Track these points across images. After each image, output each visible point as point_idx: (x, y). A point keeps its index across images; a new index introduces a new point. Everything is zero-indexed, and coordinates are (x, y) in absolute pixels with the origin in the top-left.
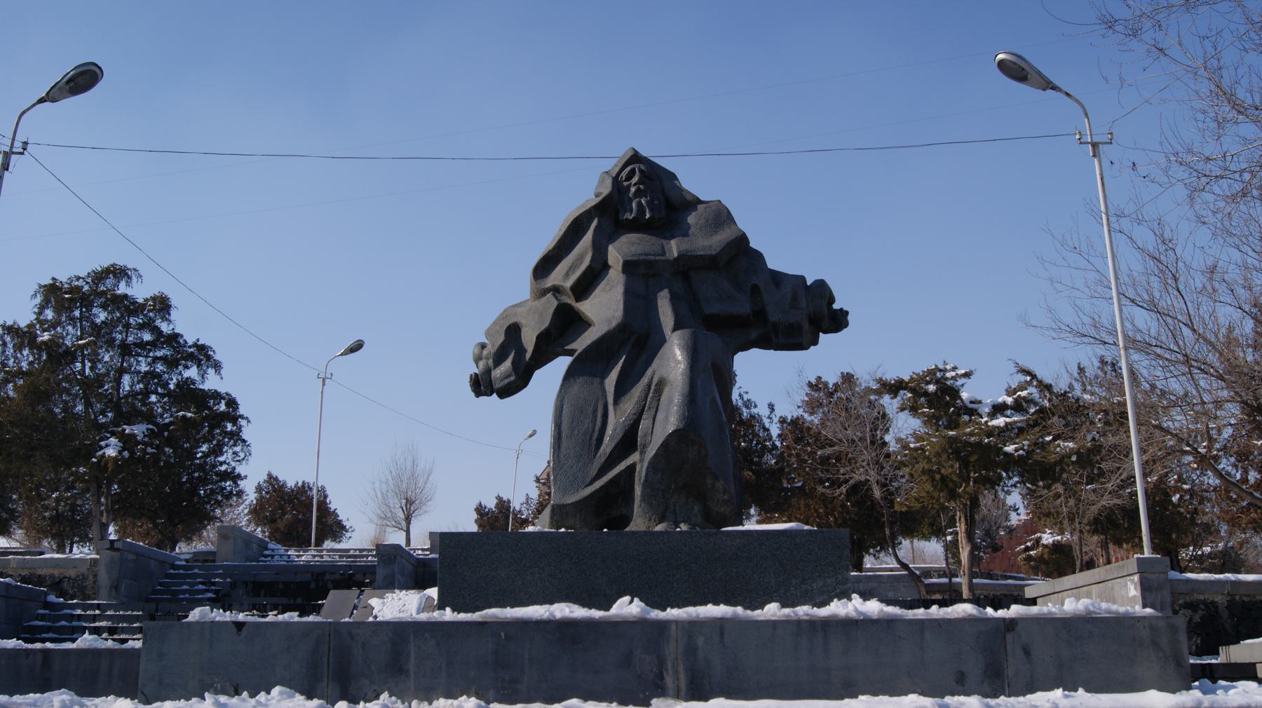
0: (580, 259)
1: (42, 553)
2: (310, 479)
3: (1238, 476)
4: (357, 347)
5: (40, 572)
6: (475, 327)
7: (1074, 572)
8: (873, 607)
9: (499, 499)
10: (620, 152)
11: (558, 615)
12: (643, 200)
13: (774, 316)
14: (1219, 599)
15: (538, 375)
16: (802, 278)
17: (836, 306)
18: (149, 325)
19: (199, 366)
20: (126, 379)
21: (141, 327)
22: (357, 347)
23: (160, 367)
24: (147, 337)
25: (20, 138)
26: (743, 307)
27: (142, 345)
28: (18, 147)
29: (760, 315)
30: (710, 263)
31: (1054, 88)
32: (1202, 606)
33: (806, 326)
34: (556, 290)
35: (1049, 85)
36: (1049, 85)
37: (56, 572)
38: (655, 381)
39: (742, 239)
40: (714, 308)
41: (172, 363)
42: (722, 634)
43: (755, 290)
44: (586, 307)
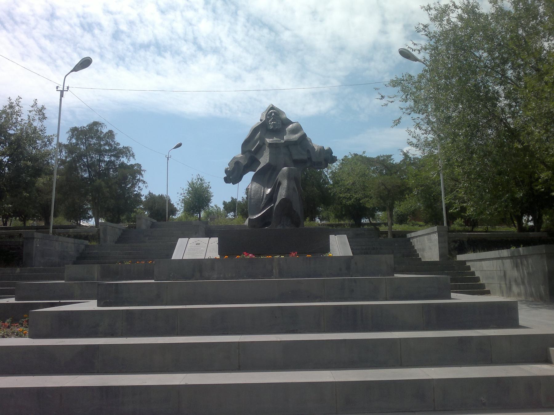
1: (55, 216)
2: (164, 194)
4: (179, 145)
9: (232, 198)
13: (314, 159)
15: (245, 177)
16: (133, 173)
18: (107, 144)
19: (127, 156)
21: (105, 145)
22: (179, 145)
23: (113, 158)
24: (107, 148)
25: (66, 85)
26: (305, 157)
27: (106, 151)
28: (65, 89)
29: (310, 159)
34: (250, 151)
37: (86, 234)
39: (304, 136)
40: (296, 157)
41: (117, 156)
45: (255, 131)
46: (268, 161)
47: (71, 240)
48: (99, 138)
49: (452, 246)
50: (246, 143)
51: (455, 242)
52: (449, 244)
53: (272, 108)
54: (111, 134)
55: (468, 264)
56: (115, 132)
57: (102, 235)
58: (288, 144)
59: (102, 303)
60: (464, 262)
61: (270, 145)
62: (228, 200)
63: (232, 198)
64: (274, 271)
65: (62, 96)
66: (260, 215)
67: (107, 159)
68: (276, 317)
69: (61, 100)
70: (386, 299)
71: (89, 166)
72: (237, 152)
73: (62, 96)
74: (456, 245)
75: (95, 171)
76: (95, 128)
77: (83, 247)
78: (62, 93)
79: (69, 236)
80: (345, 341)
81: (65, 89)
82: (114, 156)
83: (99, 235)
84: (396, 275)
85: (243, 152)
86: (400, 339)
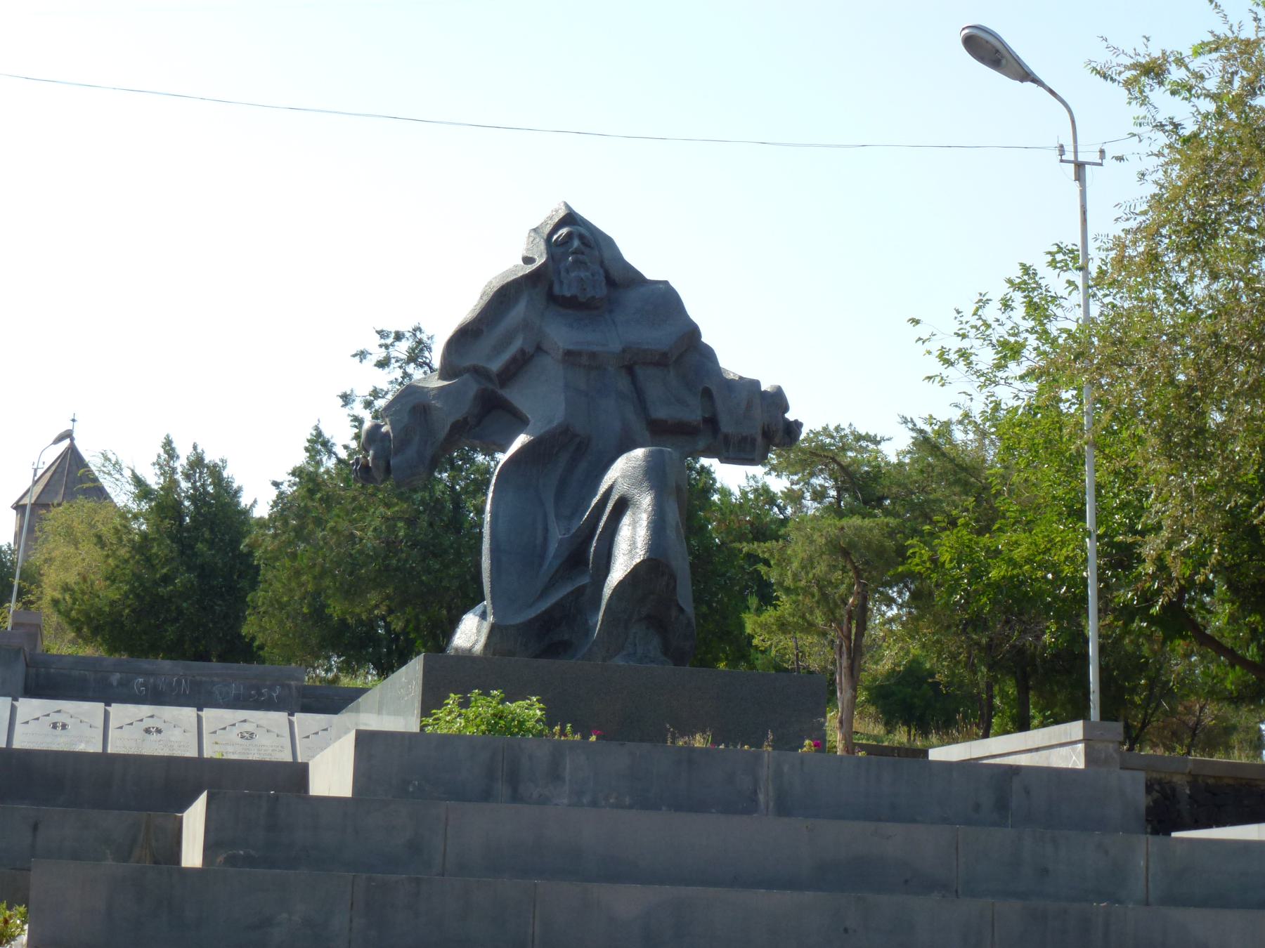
3: (1167, 241)
7: (986, 735)
10: (545, 212)
11: (120, 744)
12: (576, 279)
13: (726, 426)
14: (1178, 780)
16: (756, 384)
17: (790, 416)
20: (889, 612)
26: (694, 413)
29: (712, 422)
30: (662, 361)
31: (1036, 80)
32: (1157, 787)
33: (759, 439)
34: (478, 372)
35: (1025, 75)
36: (1025, 75)
43: (707, 393)
44: (517, 396)
45: (503, 298)
53: (570, 218)
61: (571, 357)
64: (761, 797)
66: (1093, 650)
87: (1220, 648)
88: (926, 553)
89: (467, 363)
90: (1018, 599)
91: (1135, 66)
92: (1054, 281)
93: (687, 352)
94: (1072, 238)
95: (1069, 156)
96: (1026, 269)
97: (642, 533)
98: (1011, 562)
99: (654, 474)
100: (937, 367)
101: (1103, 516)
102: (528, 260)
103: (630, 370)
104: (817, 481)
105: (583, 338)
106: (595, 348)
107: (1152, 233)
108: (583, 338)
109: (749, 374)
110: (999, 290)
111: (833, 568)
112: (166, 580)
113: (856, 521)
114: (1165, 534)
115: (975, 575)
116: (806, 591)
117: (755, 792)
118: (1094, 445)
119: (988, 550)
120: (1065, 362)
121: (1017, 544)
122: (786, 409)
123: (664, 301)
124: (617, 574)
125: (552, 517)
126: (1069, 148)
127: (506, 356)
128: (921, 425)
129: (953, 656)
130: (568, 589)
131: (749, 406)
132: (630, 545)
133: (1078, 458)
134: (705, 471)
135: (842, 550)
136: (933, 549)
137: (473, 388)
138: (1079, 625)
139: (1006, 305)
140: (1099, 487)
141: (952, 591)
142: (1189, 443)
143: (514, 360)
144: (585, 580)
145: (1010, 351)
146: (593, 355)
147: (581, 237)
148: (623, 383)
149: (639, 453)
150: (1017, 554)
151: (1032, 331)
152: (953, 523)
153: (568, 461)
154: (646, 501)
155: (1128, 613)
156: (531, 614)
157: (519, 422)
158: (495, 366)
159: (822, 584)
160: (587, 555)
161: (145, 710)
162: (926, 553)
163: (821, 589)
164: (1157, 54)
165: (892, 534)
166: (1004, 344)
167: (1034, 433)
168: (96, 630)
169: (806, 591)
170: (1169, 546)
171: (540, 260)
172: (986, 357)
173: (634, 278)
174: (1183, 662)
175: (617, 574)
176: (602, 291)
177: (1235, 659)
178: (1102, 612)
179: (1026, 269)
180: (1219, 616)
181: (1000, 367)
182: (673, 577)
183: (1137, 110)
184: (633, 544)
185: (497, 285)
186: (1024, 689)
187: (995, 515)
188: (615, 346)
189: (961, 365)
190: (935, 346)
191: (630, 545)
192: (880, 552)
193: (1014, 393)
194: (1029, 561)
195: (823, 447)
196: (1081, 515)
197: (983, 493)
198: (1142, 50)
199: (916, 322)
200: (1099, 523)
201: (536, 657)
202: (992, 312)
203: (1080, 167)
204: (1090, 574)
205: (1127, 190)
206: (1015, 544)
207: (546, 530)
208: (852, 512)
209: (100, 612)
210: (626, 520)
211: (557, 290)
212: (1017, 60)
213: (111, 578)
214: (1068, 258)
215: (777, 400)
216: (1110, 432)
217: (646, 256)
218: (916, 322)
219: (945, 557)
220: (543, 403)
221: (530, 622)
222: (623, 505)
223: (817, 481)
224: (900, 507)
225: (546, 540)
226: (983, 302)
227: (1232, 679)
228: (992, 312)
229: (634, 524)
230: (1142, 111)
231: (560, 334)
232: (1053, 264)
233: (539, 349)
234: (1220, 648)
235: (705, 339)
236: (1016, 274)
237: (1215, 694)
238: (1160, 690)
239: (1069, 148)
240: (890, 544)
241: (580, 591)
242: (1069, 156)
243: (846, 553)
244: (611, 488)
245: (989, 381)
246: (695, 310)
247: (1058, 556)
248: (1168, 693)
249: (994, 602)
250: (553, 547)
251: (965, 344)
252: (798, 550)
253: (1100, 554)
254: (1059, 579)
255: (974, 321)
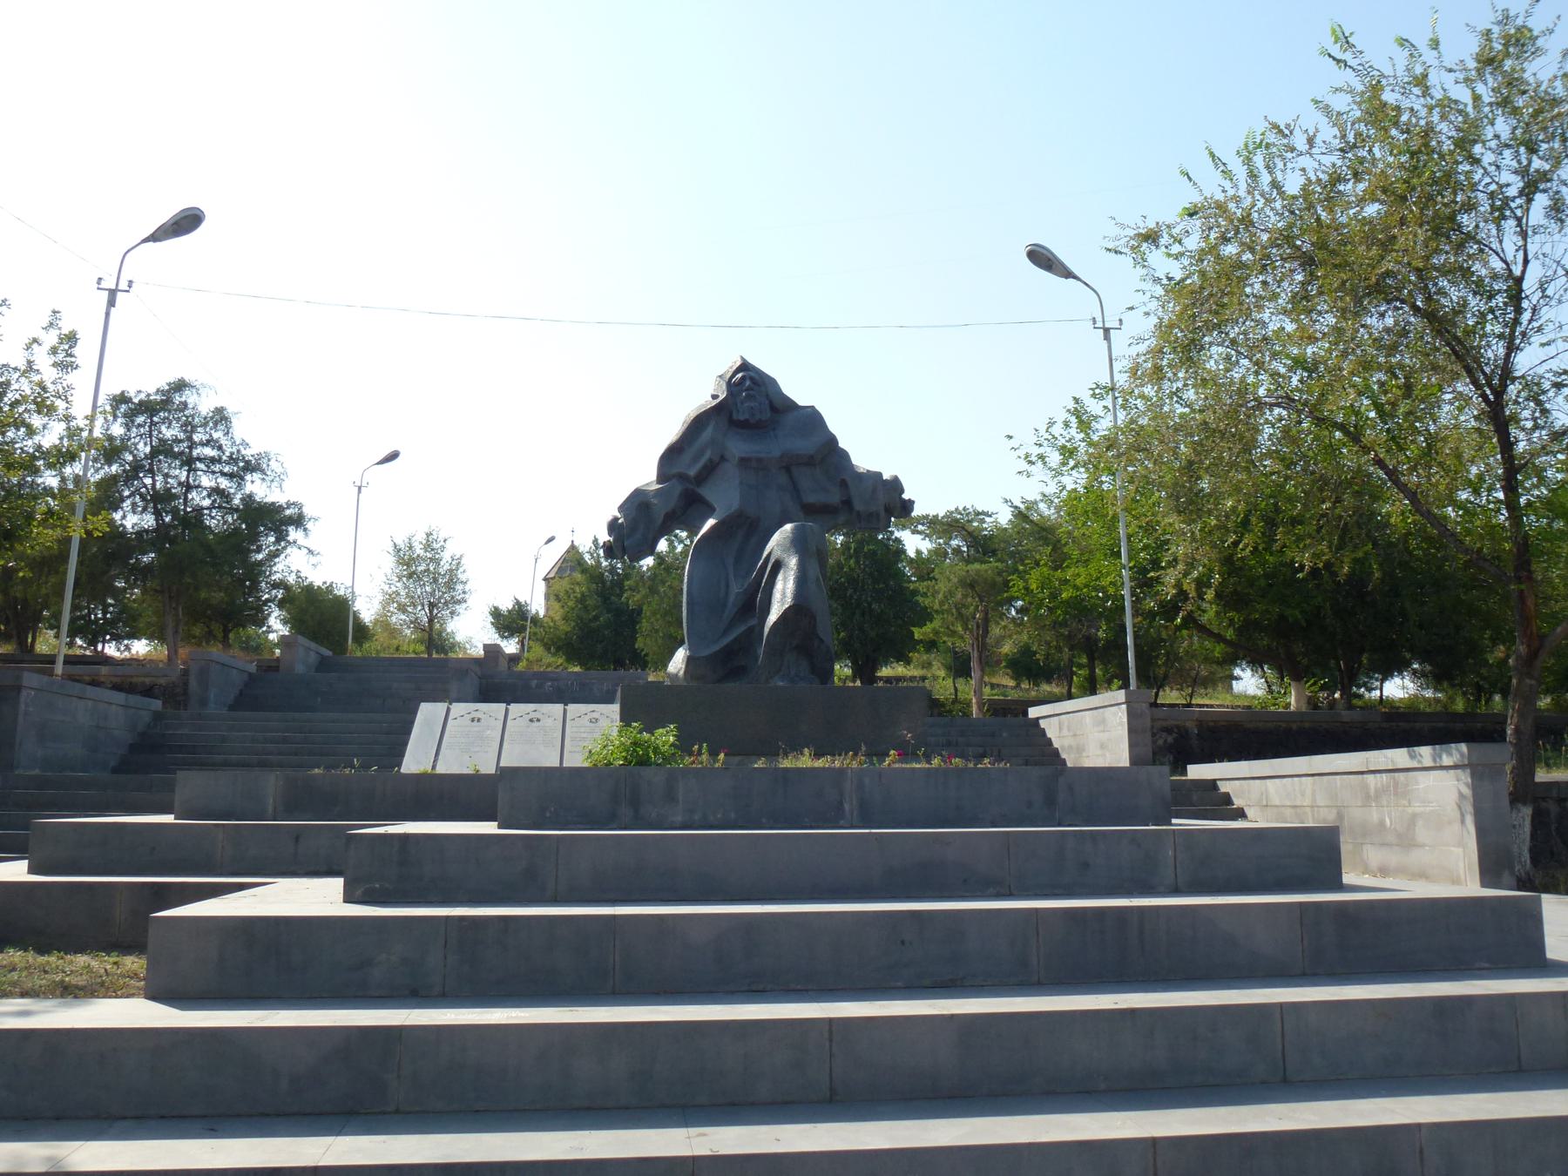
0: (702, 452)
5: (134, 680)
6: (63, 315)
8: (489, 828)
10: (728, 364)
13: (858, 506)
14: (1189, 724)
16: (880, 474)
17: (906, 496)
26: (835, 498)
28: (123, 285)
29: (847, 503)
30: (810, 461)
31: (1075, 277)
33: (882, 513)
34: (682, 477)
35: (1068, 274)
36: (1068, 274)
37: (148, 680)
38: (772, 560)
40: (811, 498)
42: (297, 839)
44: (707, 492)
45: (698, 425)
46: (735, 505)
47: (120, 697)
48: (189, 427)
49: (1160, 742)
50: (671, 456)
51: (1168, 730)
52: (1154, 735)
53: (745, 366)
54: (220, 417)
55: (1224, 787)
56: (230, 409)
57: (193, 684)
58: (789, 464)
59: (359, 892)
60: (1212, 785)
61: (744, 462)
62: (506, 605)
63: (518, 603)
64: (847, 807)
65: (111, 303)
66: (1130, 640)
67: (206, 481)
68: (903, 943)
69: (107, 314)
70: (1176, 891)
71: (159, 500)
72: (645, 474)
73: (111, 303)
74: (1170, 739)
75: (175, 512)
76: (177, 399)
77: (146, 717)
78: (113, 294)
79: (95, 683)
80: (1132, 1013)
81: (123, 285)
82: (231, 476)
83: (186, 684)
84: (1179, 823)
85: (661, 477)
86: (1281, 1005)
87: (1210, 633)
88: (1021, 584)
89: (675, 471)
90: (1081, 609)
91: (1139, 235)
92: (1094, 407)
93: (830, 454)
94: (1105, 380)
95: (1099, 324)
96: (1076, 400)
97: (791, 585)
98: (1076, 587)
99: (799, 543)
100: (1024, 466)
101: (1130, 550)
102: (714, 397)
103: (788, 469)
104: (954, 543)
105: (753, 449)
106: (762, 455)
107: (1158, 352)
108: (753, 449)
109: (874, 468)
110: (1062, 415)
111: (965, 596)
112: (596, 618)
113: (977, 566)
114: (1181, 567)
115: (1053, 596)
116: (949, 611)
117: (841, 803)
118: (1126, 510)
119: (1060, 580)
120: (1106, 454)
121: (1078, 575)
122: (902, 491)
123: (812, 419)
124: (773, 617)
125: (731, 577)
126: (1099, 319)
127: (699, 466)
128: (1017, 503)
129: (1048, 643)
130: (742, 628)
131: (874, 491)
132: (784, 592)
133: (1115, 518)
134: (898, 541)
135: (970, 584)
136: (1026, 581)
137: (678, 489)
138: (1109, 682)
139: (1067, 424)
140: (1129, 537)
141: (1039, 607)
142: (1191, 505)
143: (705, 467)
144: (753, 622)
145: (1068, 452)
146: (759, 460)
147: (752, 379)
148: (783, 479)
149: (788, 527)
150: (1079, 582)
151: (1083, 440)
152: (1037, 564)
153: (744, 533)
154: (793, 562)
155: (1151, 615)
156: (716, 648)
157: (709, 511)
158: (692, 472)
159: (959, 607)
160: (756, 600)
161: (532, 706)
162: (1021, 584)
163: (958, 610)
164: (1152, 225)
165: (1000, 574)
166: (1063, 447)
167: (1086, 506)
168: (558, 649)
169: (949, 611)
170: (1186, 575)
171: (722, 397)
172: (1055, 458)
173: (791, 406)
174: (1189, 642)
175: (773, 617)
176: (768, 415)
177: (1219, 638)
178: (1136, 614)
179: (1076, 400)
180: (1210, 613)
181: (1064, 464)
182: (813, 617)
183: (1141, 271)
184: (784, 595)
185: (693, 415)
186: (1092, 659)
187: (1066, 557)
188: (776, 453)
189: (1040, 463)
190: (1022, 453)
191: (784, 592)
192: (993, 584)
193: (1076, 480)
194: (1086, 586)
195: (957, 521)
196: (1118, 555)
197: (1057, 546)
198: (1141, 225)
199: (1010, 437)
200: (1130, 560)
201: (719, 681)
202: (1057, 430)
203: (1107, 331)
204: (1126, 592)
205: (1139, 329)
206: (1078, 575)
207: (727, 586)
208: (976, 560)
209: (559, 639)
210: (780, 577)
211: (735, 417)
212: (1062, 265)
213: (565, 618)
214: (1099, 391)
215: (895, 485)
216: (1134, 500)
217: (797, 389)
218: (1010, 437)
219: (1034, 586)
220: (725, 496)
221: (716, 654)
222: (778, 566)
223: (954, 543)
224: (995, 555)
225: (727, 594)
226: (1051, 424)
227: (1218, 650)
228: (1057, 430)
229: (785, 579)
230: (1144, 271)
231: (737, 447)
232: (1094, 396)
233: (723, 458)
234: (1210, 633)
235: (841, 445)
236: (1071, 405)
237: (1207, 660)
238: (1172, 657)
239: (1099, 319)
240: (1000, 579)
241: (751, 630)
242: (1099, 324)
243: (972, 586)
244: (769, 554)
245: (1058, 473)
246: (833, 425)
247: (1104, 582)
248: (1178, 659)
249: (1066, 613)
250: (732, 598)
251: (1041, 450)
252: (942, 587)
253: (1132, 579)
254: (1107, 597)
255: (1047, 436)
